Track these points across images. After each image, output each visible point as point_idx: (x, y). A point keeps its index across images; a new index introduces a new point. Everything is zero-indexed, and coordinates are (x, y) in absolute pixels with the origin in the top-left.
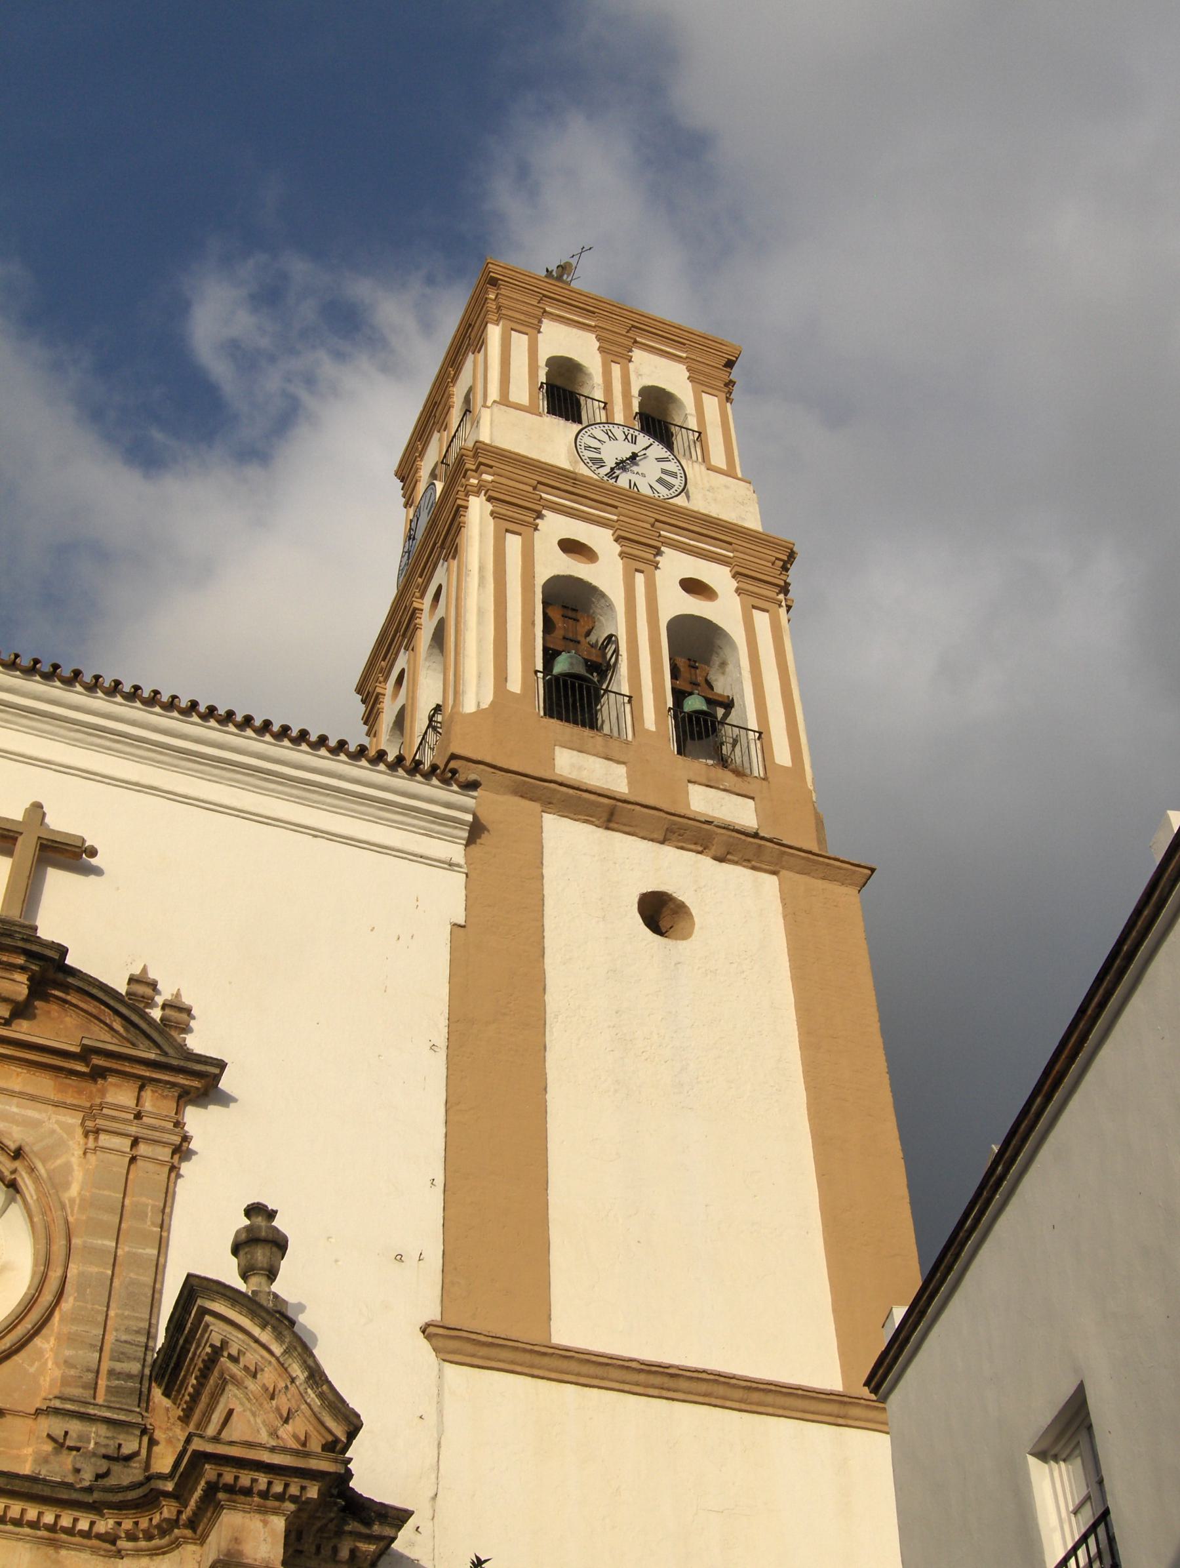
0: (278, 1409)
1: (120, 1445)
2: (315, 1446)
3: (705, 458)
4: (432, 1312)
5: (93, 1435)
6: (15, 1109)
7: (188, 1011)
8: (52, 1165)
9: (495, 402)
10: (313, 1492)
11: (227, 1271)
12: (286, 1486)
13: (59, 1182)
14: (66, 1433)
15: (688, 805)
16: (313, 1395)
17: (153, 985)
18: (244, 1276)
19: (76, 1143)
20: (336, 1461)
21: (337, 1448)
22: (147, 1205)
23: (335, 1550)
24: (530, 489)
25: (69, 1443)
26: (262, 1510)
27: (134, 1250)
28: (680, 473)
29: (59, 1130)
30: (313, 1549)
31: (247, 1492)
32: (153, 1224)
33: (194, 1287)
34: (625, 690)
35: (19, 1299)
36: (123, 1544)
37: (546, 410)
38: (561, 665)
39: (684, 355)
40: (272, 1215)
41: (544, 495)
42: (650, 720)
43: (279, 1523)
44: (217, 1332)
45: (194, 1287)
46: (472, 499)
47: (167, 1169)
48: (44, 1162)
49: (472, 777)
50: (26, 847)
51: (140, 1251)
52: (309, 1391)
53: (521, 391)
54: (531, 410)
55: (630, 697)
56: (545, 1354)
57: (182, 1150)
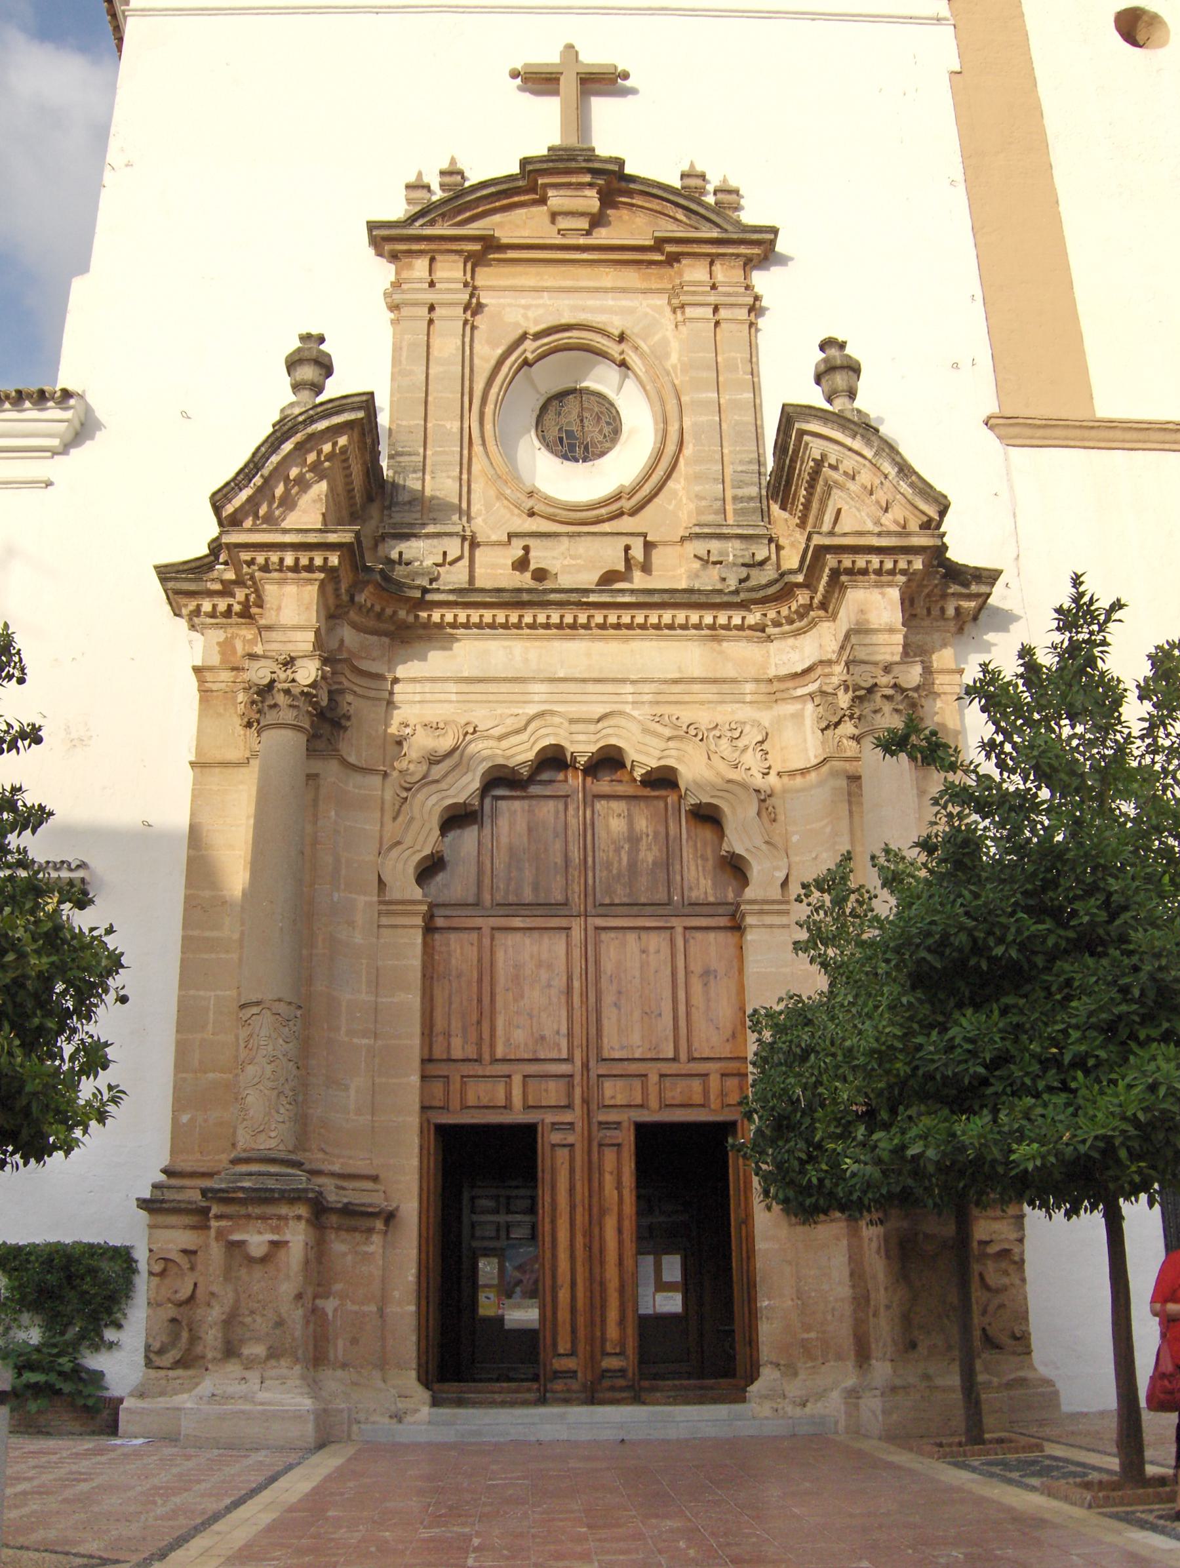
0: (878, 502)
2: (913, 526)
4: (991, 407)
6: (611, 303)
14: (709, 552)
18: (829, 400)
20: (933, 536)
21: (931, 525)
23: (943, 610)
25: (712, 559)
29: (651, 312)
30: (925, 612)
31: (864, 572)
32: (745, 373)
33: (790, 416)
36: (770, 630)
43: (894, 594)
50: (569, 84)
56: (1092, 428)
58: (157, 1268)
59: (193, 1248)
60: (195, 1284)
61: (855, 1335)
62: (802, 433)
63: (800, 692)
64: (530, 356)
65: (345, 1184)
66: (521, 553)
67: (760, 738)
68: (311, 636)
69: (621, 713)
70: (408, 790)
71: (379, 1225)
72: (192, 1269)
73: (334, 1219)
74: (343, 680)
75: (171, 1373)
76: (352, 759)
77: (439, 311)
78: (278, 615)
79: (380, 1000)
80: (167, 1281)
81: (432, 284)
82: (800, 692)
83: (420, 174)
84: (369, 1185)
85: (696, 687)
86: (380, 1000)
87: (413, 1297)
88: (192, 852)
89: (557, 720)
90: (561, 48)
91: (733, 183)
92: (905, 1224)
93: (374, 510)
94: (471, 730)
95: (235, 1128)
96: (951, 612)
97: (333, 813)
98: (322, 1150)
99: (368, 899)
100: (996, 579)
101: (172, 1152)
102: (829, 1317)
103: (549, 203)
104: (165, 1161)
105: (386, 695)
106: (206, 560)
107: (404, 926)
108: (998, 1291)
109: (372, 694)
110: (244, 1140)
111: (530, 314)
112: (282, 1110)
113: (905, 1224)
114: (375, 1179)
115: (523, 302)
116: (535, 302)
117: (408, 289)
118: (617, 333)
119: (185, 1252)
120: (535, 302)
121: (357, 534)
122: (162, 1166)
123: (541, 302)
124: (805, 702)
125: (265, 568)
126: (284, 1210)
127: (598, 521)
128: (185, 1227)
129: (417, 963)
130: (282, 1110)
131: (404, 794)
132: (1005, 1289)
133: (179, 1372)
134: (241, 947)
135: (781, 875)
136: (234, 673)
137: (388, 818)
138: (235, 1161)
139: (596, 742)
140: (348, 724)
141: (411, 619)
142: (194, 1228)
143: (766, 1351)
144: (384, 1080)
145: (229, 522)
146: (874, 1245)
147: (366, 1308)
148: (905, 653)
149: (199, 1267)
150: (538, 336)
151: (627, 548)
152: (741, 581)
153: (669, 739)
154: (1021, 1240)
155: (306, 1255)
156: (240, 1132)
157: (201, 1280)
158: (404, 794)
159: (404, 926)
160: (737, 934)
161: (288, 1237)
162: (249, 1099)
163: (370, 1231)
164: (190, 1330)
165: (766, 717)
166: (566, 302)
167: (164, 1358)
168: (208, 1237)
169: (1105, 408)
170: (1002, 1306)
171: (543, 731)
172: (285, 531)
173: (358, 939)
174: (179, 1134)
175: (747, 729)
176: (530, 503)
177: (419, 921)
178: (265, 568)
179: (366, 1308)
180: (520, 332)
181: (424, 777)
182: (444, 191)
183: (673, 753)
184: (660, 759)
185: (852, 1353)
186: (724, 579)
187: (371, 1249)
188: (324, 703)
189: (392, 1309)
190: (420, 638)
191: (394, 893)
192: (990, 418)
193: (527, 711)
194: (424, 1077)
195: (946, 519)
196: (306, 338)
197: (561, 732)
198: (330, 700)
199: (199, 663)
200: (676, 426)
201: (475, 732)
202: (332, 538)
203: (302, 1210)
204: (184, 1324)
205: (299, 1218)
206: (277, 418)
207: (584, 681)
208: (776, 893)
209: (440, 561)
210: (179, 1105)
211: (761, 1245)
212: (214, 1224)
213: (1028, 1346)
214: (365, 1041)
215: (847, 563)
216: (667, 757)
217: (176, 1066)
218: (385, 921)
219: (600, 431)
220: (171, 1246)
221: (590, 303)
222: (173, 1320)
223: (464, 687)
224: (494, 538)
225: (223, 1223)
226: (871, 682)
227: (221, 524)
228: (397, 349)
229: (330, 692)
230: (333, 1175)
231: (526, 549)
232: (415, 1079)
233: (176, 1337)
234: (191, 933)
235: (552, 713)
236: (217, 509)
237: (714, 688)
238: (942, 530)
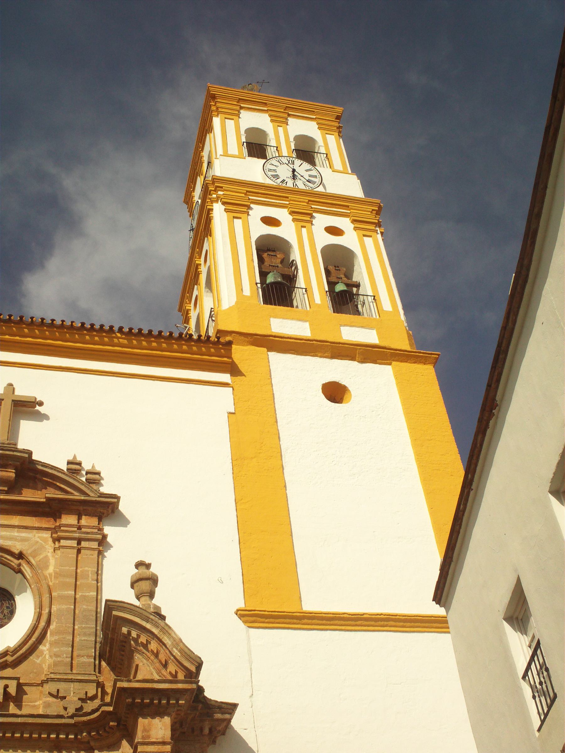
1: (86, 692)
4: (241, 605)
5: (72, 689)
6: (16, 534)
15: (341, 337)
16: (176, 651)
18: (138, 598)
22: (88, 571)
23: (202, 729)
25: (60, 695)
27: (84, 594)
32: (93, 580)
34: (303, 286)
40: (148, 566)
51: (87, 594)
52: (174, 649)
77: (83, 544)
151: (6, 687)
152: (77, 710)
186: (65, 709)
192: (238, 610)
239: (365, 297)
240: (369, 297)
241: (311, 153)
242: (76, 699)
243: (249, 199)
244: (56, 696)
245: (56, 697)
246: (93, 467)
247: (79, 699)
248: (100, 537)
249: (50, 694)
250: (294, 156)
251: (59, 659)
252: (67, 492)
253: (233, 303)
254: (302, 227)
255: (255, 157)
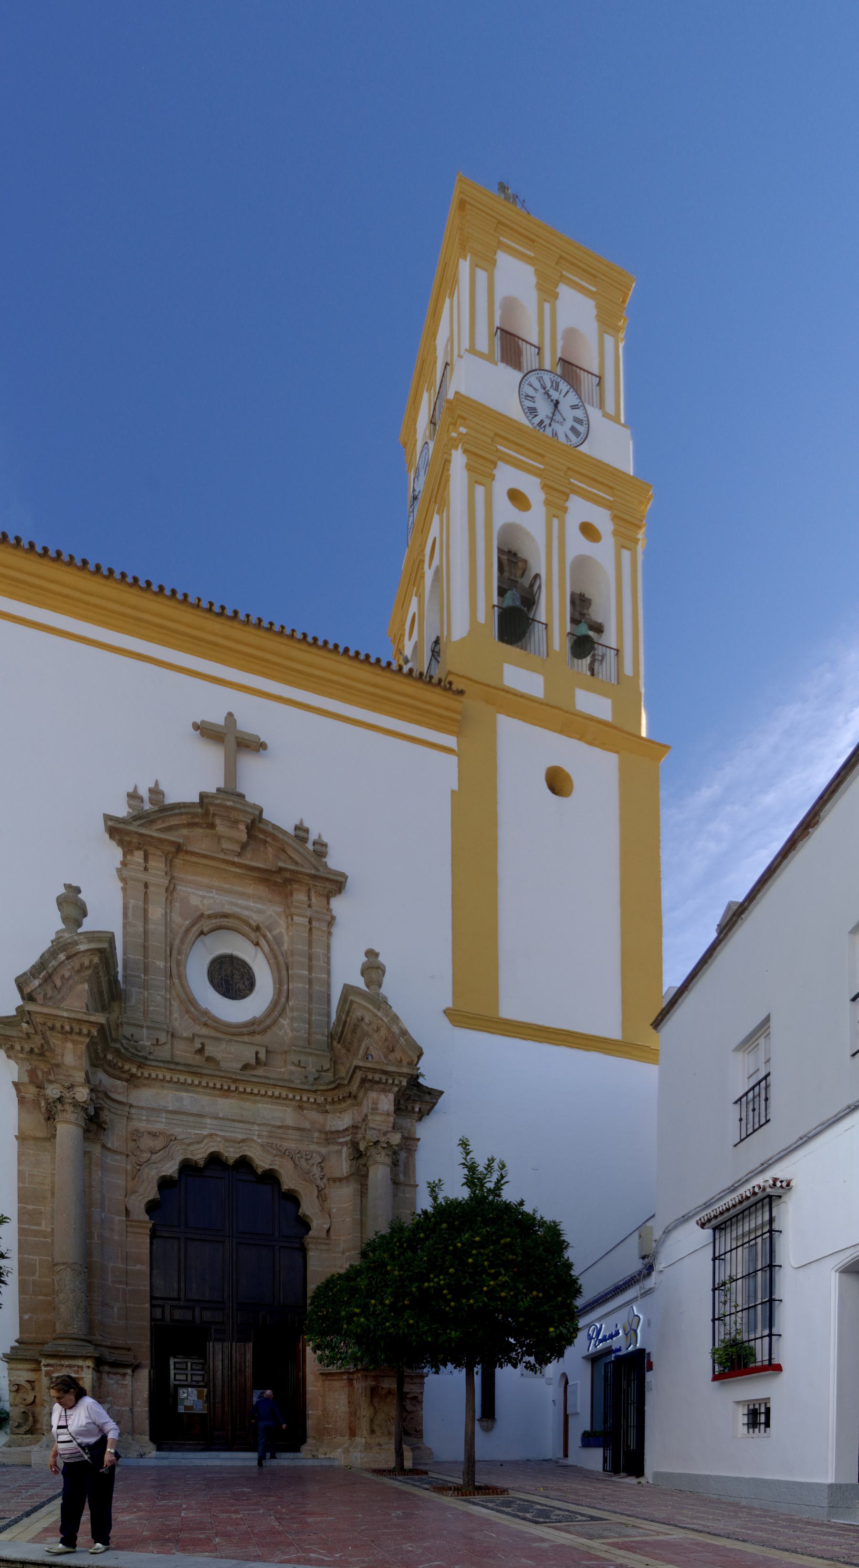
1: (322, 1066)
2: (405, 1063)
3: (601, 406)
4: (449, 1004)
6: (252, 904)
7: (325, 845)
8: (276, 932)
9: (466, 350)
10: (404, 1083)
11: (359, 982)
12: (394, 1080)
13: (278, 940)
14: (299, 1061)
15: (574, 704)
17: (307, 831)
18: (368, 986)
19: (282, 922)
20: (413, 1069)
21: (413, 1064)
23: (413, 1108)
24: (489, 441)
26: (384, 1091)
28: (583, 436)
29: (274, 915)
32: (324, 962)
33: (348, 990)
34: (543, 620)
35: (616, 466)
36: (328, 1107)
37: (499, 359)
38: (508, 602)
39: (594, 289)
41: (499, 447)
42: (556, 645)
43: (391, 1097)
44: (358, 1013)
45: (348, 990)
46: (454, 452)
47: (326, 934)
48: (270, 932)
49: (461, 687)
50: (231, 740)
53: (483, 344)
54: (488, 358)
55: (546, 625)
56: (496, 1022)
57: (331, 922)
58: (14, 1388)
59: (33, 1380)
60: (35, 1397)
61: (349, 1427)
62: (352, 1002)
63: (341, 1140)
64: (205, 930)
65: (113, 1351)
66: (200, 1046)
67: (320, 1160)
68: (83, 1074)
69: (252, 1140)
70: (140, 1165)
71: (129, 1371)
72: (33, 1389)
73: (106, 1369)
74: (102, 1102)
75: (24, 1436)
76: (109, 1145)
78: (62, 1059)
79: (129, 1267)
80: (20, 1395)
81: (146, 869)
82: (341, 1140)
83: (136, 788)
84: (125, 1352)
85: (290, 1131)
86: (129, 1267)
87: (147, 1404)
88: (21, 1185)
89: (219, 1139)
90: (225, 715)
91: (325, 839)
92: (374, 1383)
93: (115, 1005)
94: (173, 1139)
95: (55, 1324)
96: (417, 1109)
97: (100, 1173)
98: (101, 1336)
99: (121, 1218)
100: (440, 1096)
101: (20, 1332)
102: (338, 1419)
103: (217, 828)
104: (17, 1336)
105: (127, 1114)
106: (16, 1019)
107: (140, 1233)
108: (410, 1413)
109: (119, 1112)
110: (59, 1328)
111: (205, 902)
112: (79, 1315)
113: (374, 1383)
114: (129, 1350)
115: (201, 893)
116: (208, 895)
117: (132, 869)
118: (254, 924)
119: (28, 1381)
120: (208, 895)
121: (108, 1019)
122: (16, 1339)
123: (211, 895)
124: (343, 1146)
125: (52, 1028)
126: (80, 1362)
127: (242, 1034)
128: (28, 1370)
129: (148, 1251)
130: (79, 1315)
131: (139, 1168)
132: (414, 1412)
133: (29, 1436)
134: (53, 1236)
135: (326, 1226)
136: (38, 1089)
137: (129, 1179)
138: (55, 1339)
139: (238, 1153)
140: (106, 1127)
141: (139, 1074)
142: (32, 1370)
143: (310, 1432)
144: (132, 1305)
145: (29, 998)
146: (360, 1391)
147: (124, 1408)
148: (394, 1127)
149: (37, 1388)
150: (210, 917)
151: (257, 1053)
152: (315, 1079)
153: (275, 1156)
154: (422, 1393)
155: (93, 1384)
156: (58, 1325)
157: (38, 1394)
158: (139, 1168)
159: (140, 1233)
160: (33, 994)
161: (83, 1375)
162: (62, 1309)
163: (124, 1375)
164: (34, 1417)
165: (323, 1150)
166: (226, 898)
167: (20, 1429)
168: (41, 1375)
169: (509, 1010)
170: (412, 1418)
171: (211, 1144)
172: (64, 1010)
173: (116, 1238)
174: (23, 1324)
175: (315, 1155)
176: (204, 1019)
177: (148, 1231)
178: (52, 1028)
179: (124, 1408)
180: (198, 913)
181: (149, 1160)
182: (151, 803)
183: (277, 1163)
184: (270, 1165)
185: (348, 1434)
187: (126, 1383)
188: (92, 1113)
189: (137, 1409)
190: (145, 1085)
191: (134, 1216)
193: (203, 1132)
194: (152, 1306)
195: (420, 1062)
196: (68, 887)
197: (221, 1145)
198: (96, 1112)
199: (16, 1080)
200: (285, 987)
201: (176, 1139)
202: (93, 1019)
203: (89, 1363)
204: (30, 1414)
205: (89, 1367)
206: (53, 937)
207: (233, 1120)
208: (324, 1234)
209: (155, 1042)
210: (22, 1311)
211: (309, 1388)
212: (44, 1369)
213: (422, 1435)
214: (121, 1286)
215: (370, 1077)
216: (274, 1164)
217: (19, 1291)
218: (129, 1229)
219: (244, 984)
220: (21, 1378)
221: (240, 902)
222: (24, 1412)
223: (170, 1116)
224: (185, 1035)
225: (48, 1368)
226: (376, 1139)
227: (23, 998)
228: (125, 908)
229: (95, 1108)
230: (107, 1347)
231: (203, 1044)
232: (147, 1305)
233: (26, 1419)
234: (23, 1226)
235: (217, 1135)
236: (20, 989)
237: (299, 1133)
238: (418, 1066)
239: (608, 649)
240: (612, 651)
241: (578, 370)
242: (314, 1070)
243: (498, 450)
244: (299, 1064)
245: (299, 1065)
246: (320, 836)
247: (317, 1071)
248: (328, 918)
249: (293, 1064)
250: (559, 373)
251: (298, 1034)
252: (297, 863)
253: (464, 634)
254: (555, 516)
255: (511, 366)
